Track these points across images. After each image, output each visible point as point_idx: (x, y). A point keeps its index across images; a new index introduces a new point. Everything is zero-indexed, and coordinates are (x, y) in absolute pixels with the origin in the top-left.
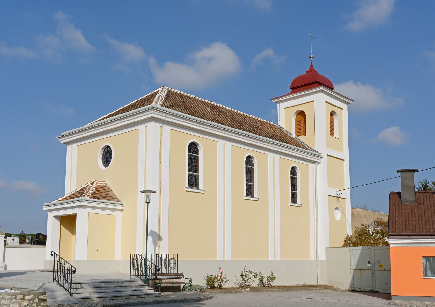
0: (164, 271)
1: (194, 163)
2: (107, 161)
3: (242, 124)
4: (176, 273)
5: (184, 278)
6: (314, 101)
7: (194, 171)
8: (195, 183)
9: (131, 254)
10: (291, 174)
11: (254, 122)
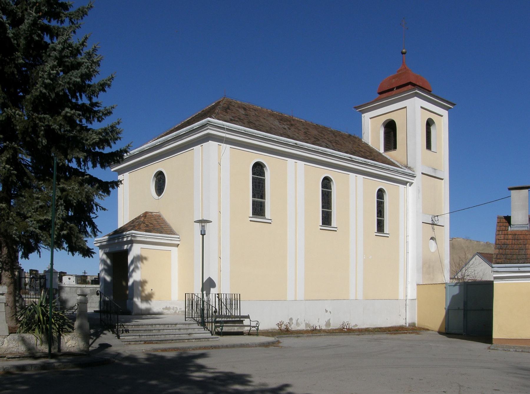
0: (224, 312)
1: (259, 187)
2: (160, 189)
3: (318, 139)
4: (239, 315)
5: (250, 320)
6: (406, 107)
7: (260, 197)
8: (261, 211)
9: (186, 294)
10: (377, 198)
11: (333, 136)
